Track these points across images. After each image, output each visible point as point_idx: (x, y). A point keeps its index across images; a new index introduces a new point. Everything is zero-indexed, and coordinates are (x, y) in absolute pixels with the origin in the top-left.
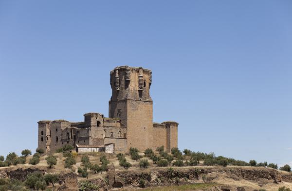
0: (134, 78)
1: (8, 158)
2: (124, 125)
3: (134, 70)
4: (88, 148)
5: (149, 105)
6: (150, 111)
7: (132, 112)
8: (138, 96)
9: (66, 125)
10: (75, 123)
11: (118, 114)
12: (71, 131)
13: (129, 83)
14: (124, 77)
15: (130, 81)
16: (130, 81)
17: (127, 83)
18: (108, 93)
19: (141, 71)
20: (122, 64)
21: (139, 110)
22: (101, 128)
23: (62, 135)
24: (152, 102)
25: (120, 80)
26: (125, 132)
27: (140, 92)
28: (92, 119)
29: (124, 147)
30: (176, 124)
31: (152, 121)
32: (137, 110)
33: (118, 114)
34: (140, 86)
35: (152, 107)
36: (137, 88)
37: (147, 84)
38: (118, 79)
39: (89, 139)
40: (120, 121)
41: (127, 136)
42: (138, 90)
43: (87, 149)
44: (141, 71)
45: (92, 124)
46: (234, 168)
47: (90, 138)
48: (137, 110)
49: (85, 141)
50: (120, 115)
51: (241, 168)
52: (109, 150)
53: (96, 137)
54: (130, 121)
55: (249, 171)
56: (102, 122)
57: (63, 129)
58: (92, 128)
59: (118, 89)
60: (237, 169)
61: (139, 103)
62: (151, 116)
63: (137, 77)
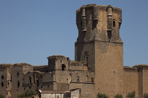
2: (91, 69)
3: (102, 8)
4: (52, 94)
5: (119, 47)
7: (100, 54)
8: (107, 37)
9: (28, 69)
12: (34, 76)
13: (97, 23)
17: (95, 22)
21: (108, 53)
22: (66, 72)
23: (23, 79)
25: (87, 20)
26: (93, 77)
29: (91, 92)
32: (106, 52)
33: (84, 58)
35: (122, 50)
36: (106, 29)
37: (117, 24)
38: (85, 18)
40: (87, 64)
41: (96, 81)
42: (106, 30)
43: (50, 94)
47: (54, 83)
50: (87, 58)
53: (60, 82)
54: (98, 65)
56: (67, 66)
57: (25, 73)
58: (57, 72)
59: (85, 30)
61: (108, 45)
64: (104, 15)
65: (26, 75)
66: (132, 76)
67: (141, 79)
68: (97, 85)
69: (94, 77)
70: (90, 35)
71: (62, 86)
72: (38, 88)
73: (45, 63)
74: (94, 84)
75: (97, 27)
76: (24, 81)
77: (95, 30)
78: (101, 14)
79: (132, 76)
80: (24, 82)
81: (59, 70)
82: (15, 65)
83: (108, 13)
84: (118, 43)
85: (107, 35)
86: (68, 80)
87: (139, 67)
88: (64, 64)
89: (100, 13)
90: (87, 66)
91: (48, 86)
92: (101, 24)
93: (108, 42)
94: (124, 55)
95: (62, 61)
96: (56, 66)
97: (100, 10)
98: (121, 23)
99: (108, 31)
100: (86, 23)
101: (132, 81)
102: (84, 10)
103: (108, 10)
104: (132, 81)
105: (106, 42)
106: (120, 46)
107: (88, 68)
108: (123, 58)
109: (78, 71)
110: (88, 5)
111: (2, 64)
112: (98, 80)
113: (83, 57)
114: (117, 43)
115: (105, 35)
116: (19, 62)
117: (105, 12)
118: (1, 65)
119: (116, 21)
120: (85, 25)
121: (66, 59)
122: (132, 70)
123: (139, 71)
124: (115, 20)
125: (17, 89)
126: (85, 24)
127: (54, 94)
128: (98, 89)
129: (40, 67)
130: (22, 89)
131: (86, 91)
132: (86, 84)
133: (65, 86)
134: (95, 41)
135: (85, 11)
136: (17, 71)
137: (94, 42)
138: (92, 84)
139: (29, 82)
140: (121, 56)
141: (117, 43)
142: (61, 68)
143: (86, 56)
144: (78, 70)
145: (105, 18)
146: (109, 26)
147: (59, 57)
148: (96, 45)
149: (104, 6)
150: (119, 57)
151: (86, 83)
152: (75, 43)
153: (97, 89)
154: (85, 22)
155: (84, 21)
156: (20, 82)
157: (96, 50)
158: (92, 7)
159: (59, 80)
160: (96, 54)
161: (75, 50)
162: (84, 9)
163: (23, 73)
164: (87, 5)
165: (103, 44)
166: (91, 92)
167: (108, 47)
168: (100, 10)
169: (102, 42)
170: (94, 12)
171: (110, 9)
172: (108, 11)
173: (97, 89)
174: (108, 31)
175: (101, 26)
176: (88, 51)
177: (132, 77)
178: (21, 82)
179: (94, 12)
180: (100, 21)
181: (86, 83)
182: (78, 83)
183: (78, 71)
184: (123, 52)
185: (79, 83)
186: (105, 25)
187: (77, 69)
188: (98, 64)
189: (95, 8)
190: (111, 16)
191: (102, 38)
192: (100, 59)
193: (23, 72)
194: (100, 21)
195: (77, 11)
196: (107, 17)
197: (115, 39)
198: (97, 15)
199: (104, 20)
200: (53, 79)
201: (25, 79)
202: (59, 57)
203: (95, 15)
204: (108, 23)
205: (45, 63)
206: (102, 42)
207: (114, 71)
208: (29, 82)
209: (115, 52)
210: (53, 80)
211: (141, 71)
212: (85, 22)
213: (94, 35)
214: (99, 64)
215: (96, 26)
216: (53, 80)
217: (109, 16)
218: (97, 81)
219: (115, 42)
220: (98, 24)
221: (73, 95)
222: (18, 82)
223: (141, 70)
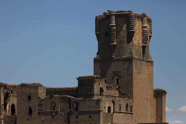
0: (138, 26)
3: (138, 17)
10: (59, 89)
11: (113, 78)
13: (133, 36)
14: (125, 25)
15: (134, 32)
16: (134, 32)
17: (130, 35)
18: (92, 47)
20: (124, 8)
23: (40, 105)
24: (153, 62)
25: (118, 31)
26: (132, 105)
27: (144, 47)
28: (95, 85)
31: (153, 88)
33: (113, 78)
38: (115, 28)
39: (99, 114)
40: (119, 87)
44: (145, 19)
45: (95, 93)
47: (101, 113)
49: (90, 117)
50: (117, 80)
56: (105, 89)
59: (115, 43)
62: (152, 85)
63: (141, 27)
65: (46, 99)
67: (160, 107)
69: (133, 105)
70: (124, 51)
71: (107, 117)
72: (69, 118)
73: (74, 84)
74: (133, 114)
75: (133, 41)
76: (41, 107)
77: (131, 44)
80: (40, 108)
82: (23, 86)
83: (143, 24)
86: (105, 108)
87: (157, 92)
88: (102, 88)
90: (118, 90)
91: (90, 117)
92: (137, 38)
95: (100, 84)
96: (94, 90)
98: (151, 36)
100: (115, 34)
102: (114, 17)
103: (143, 19)
107: (120, 92)
110: (121, 12)
111: (51, 88)
113: (111, 78)
114: (149, 62)
116: (29, 81)
118: (1, 83)
120: (115, 37)
122: (59, 91)
123: (156, 98)
125: (27, 118)
126: (115, 35)
129: (58, 89)
130: (37, 118)
132: (126, 114)
134: (133, 59)
135: (115, 19)
136: (28, 94)
137: (132, 60)
139: (52, 110)
141: (149, 62)
142: (99, 93)
143: (116, 77)
144: (111, 95)
145: (140, 29)
146: (144, 40)
148: (135, 64)
152: (94, 59)
154: (115, 33)
155: (113, 31)
156: (33, 109)
157: (134, 71)
158: (128, 15)
160: (134, 76)
161: (94, 68)
162: (114, 16)
163: (39, 97)
164: (118, 12)
169: (138, 60)
170: (131, 22)
172: (143, 21)
175: (137, 40)
176: (120, 71)
178: (35, 109)
179: (131, 22)
180: (137, 33)
182: (120, 113)
187: (110, 94)
189: (132, 16)
190: (146, 27)
193: (39, 96)
194: (137, 33)
195: (96, 17)
196: (142, 28)
198: (134, 26)
200: (100, 107)
201: (43, 106)
203: (133, 25)
204: (144, 36)
205: (74, 84)
206: (138, 60)
208: (52, 110)
210: (100, 109)
211: (160, 97)
212: (115, 33)
213: (129, 50)
215: (132, 40)
216: (100, 108)
217: (144, 27)
219: (147, 60)
220: (134, 36)
222: (28, 109)
223: (159, 96)
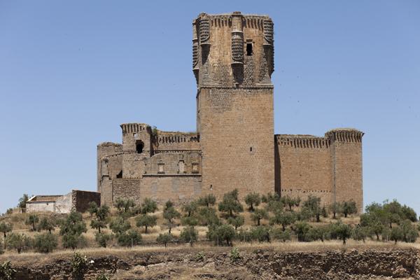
1: (368, 209)
3: (219, 21)
4: (47, 203)
5: (262, 96)
6: (265, 109)
8: (232, 78)
15: (209, 46)
16: (209, 46)
19: (236, 21)
21: (234, 110)
29: (192, 194)
30: (357, 136)
32: (229, 109)
34: (237, 52)
35: (271, 101)
36: (229, 59)
41: (205, 168)
42: (230, 64)
43: (45, 205)
46: (248, 250)
48: (229, 109)
51: (78, 258)
52: (64, 207)
53: (133, 176)
55: (302, 256)
60: (256, 252)
61: (234, 95)
64: (223, 33)
66: (314, 154)
68: (207, 177)
78: (216, 32)
79: (314, 154)
81: (129, 152)
84: (259, 88)
85: (231, 73)
89: (215, 30)
93: (235, 88)
94: (276, 111)
97: (214, 24)
99: (233, 65)
101: (312, 165)
104: (312, 165)
105: (228, 88)
106: (266, 93)
108: (273, 119)
109: (178, 151)
112: (211, 168)
114: (256, 88)
115: (226, 74)
117: (226, 28)
119: (254, 43)
121: (146, 130)
124: (251, 40)
127: (53, 204)
128: (209, 186)
131: (180, 192)
132: (181, 178)
133: (132, 185)
138: (195, 176)
140: (269, 115)
141: (256, 88)
142: (134, 148)
145: (226, 39)
147: (128, 126)
149: (223, 14)
150: (263, 118)
151: (181, 176)
153: (206, 186)
159: (130, 172)
165: (222, 94)
166: (192, 194)
167: (235, 98)
168: (214, 24)
169: (220, 88)
171: (236, 21)
173: (206, 186)
174: (233, 65)
177: (312, 156)
181: (181, 176)
183: (178, 151)
184: (273, 105)
185: (163, 176)
186: (227, 54)
187: (176, 149)
188: (209, 135)
191: (218, 82)
192: (213, 125)
197: (253, 80)
199: (223, 44)
202: (128, 126)
206: (220, 88)
207: (249, 148)
209: (253, 107)
214: (212, 135)
217: (233, 34)
218: (206, 170)
219: (252, 86)
221: (59, 206)
